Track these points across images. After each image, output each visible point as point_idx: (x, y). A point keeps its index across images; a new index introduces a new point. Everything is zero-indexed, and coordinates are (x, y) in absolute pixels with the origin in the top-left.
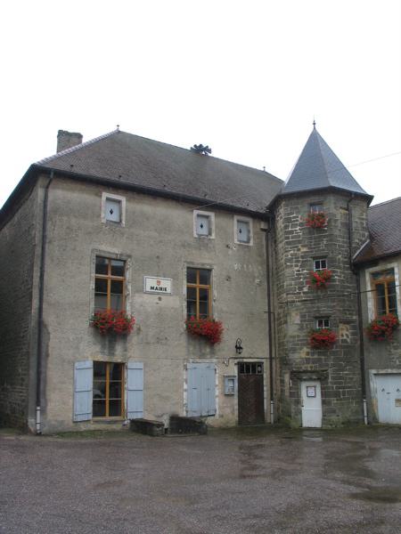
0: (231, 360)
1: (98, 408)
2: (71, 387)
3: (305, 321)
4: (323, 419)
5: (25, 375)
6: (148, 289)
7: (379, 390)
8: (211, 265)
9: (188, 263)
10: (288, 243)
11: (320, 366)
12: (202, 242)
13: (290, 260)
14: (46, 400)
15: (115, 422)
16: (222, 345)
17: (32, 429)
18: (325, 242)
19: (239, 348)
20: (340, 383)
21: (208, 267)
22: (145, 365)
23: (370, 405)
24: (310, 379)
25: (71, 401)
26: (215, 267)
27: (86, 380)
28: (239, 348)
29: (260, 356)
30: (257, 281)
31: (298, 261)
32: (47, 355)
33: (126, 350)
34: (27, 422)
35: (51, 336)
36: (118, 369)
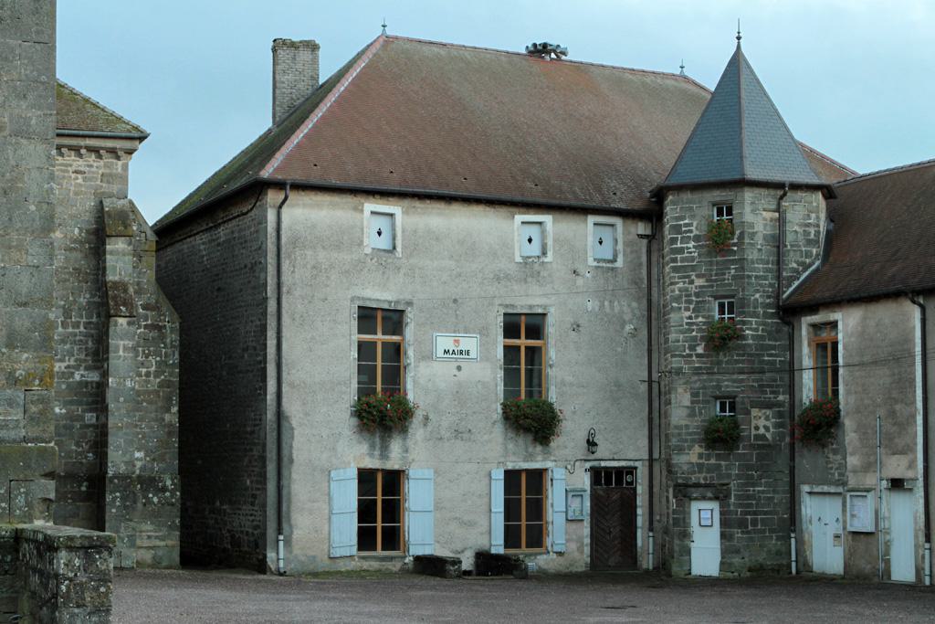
0: (577, 464)
1: (366, 539)
2: (325, 506)
3: (698, 402)
4: (722, 563)
5: (259, 489)
6: (440, 353)
7: (815, 520)
8: (545, 307)
9: (507, 306)
10: (675, 269)
11: (720, 476)
12: (531, 270)
13: (678, 299)
14: (291, 526)
15: (391, 559)
16: (564, 424)
17: (273, 567)
18: (733, 271)
19: (591, 444)
20: (750, 505)
21: (540, 311)
22: (435, 472)
23: (800, 542)
24: (704, 498)
25: (326, 527)
26: (552, 310)
27: (347, 497)
28: (591, 444)
29: (631, 457)
30: (629, 328)
31: (689, 302)
32: (291, 461)
33: (407, 451)
34: (265, 556)
35: (296, 432)
36: (394, 480)
